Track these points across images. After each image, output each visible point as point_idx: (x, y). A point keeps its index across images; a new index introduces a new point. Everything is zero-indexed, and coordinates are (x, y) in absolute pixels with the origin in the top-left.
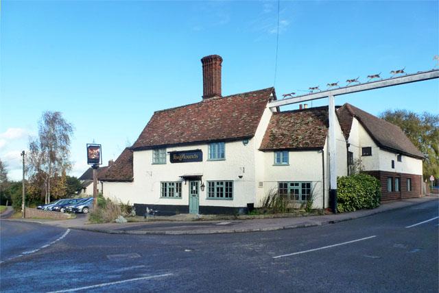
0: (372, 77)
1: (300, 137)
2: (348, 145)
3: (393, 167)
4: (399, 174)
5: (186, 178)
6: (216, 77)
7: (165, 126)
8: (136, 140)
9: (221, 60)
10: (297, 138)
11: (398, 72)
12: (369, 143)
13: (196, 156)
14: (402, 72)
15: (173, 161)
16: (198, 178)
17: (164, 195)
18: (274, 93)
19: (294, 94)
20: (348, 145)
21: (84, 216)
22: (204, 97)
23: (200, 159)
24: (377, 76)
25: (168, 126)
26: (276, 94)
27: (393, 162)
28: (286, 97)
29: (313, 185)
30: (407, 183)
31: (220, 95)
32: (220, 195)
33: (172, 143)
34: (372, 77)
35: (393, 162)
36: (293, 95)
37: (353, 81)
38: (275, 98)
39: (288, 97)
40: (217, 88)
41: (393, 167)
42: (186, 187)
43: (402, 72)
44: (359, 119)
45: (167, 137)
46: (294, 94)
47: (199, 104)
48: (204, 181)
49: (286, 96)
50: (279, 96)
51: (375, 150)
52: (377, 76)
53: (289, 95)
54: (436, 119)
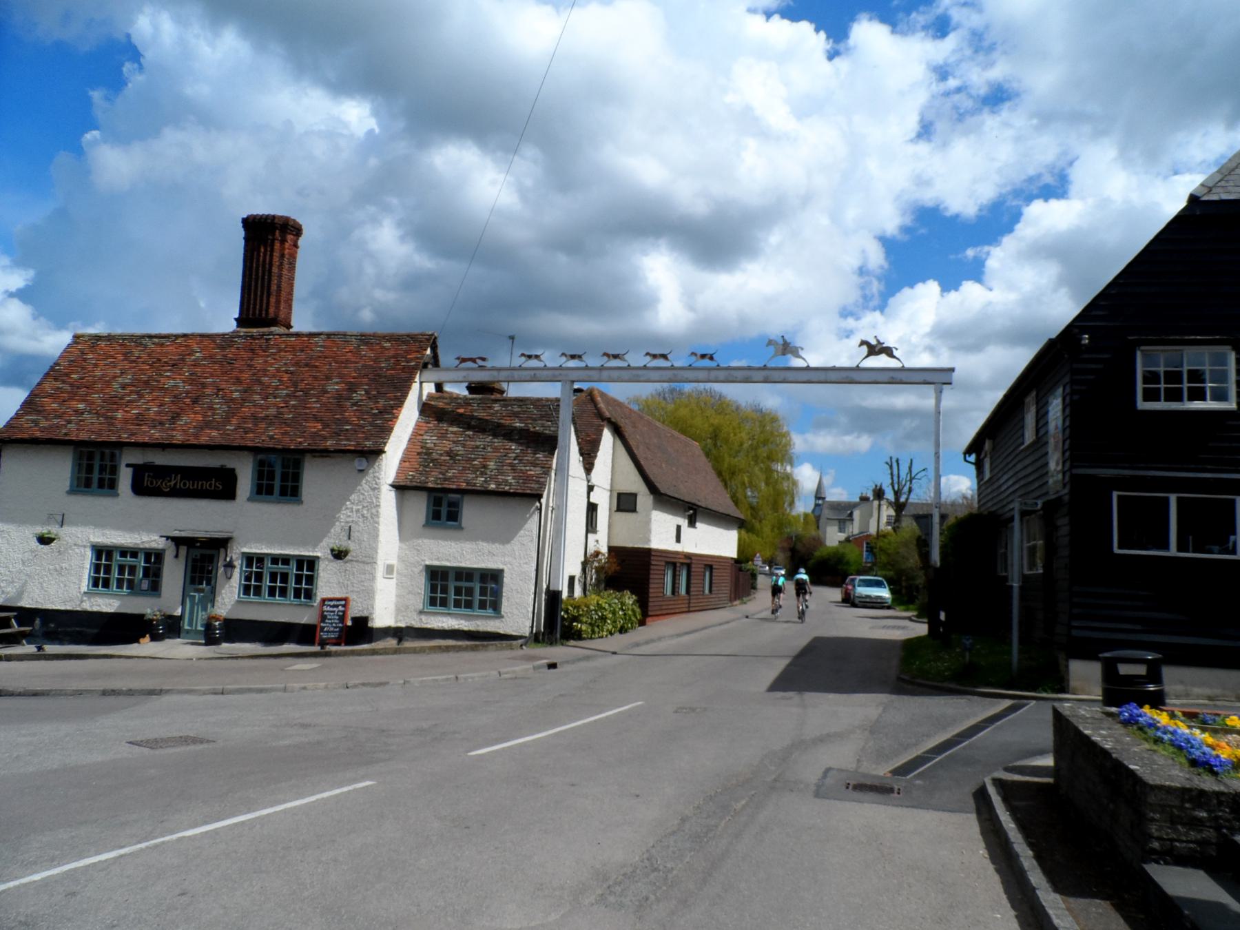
0: (655, 356)
1: (492, 465)
2: (590, 489)
3: (678, 539)
4: (689, 556)
5: (178, 541)
6: (280, 276)
7: (115, 385)
8: (12, 414)
9: (297, 231)
10: (485, 467)
11: (703, 356)
12: (633, 483)
13: (214, 484)
14: (711, 358)
15: (139, 489)
16: (222, 543)
17: (100, 581)
18: (434, 348)
19: (483, 359)
20: (590, 489)
21: (313, 609)
22: (241, 322)
23: (228, 493)
24: (664, 357)
25: (124, 387)
26: (440, 352)
27: (679, 528)
28: (463, 365)
29: (454, 579)
30: (704, 576)
31: (289, 326)
32: (464, 574)
33: (140, 439)
34: (655, 356)
35: (679, 528)
36: (480, 363)
37: (616, 357)
38: (435, 362)
39: (470, 364)
40: (282, 306)
41: (678, 539)
42: (173, 574)
43: (711, 358)
44: (618, 431)
45: (126, 421)
46: (483, 359)
47: (225, 340)
48: (235, 553)
49: (464, 360)
50: (446, 358)
51: (645, 499)
52: (664, 357)
53: (473, 360)
54: (4, 268)
